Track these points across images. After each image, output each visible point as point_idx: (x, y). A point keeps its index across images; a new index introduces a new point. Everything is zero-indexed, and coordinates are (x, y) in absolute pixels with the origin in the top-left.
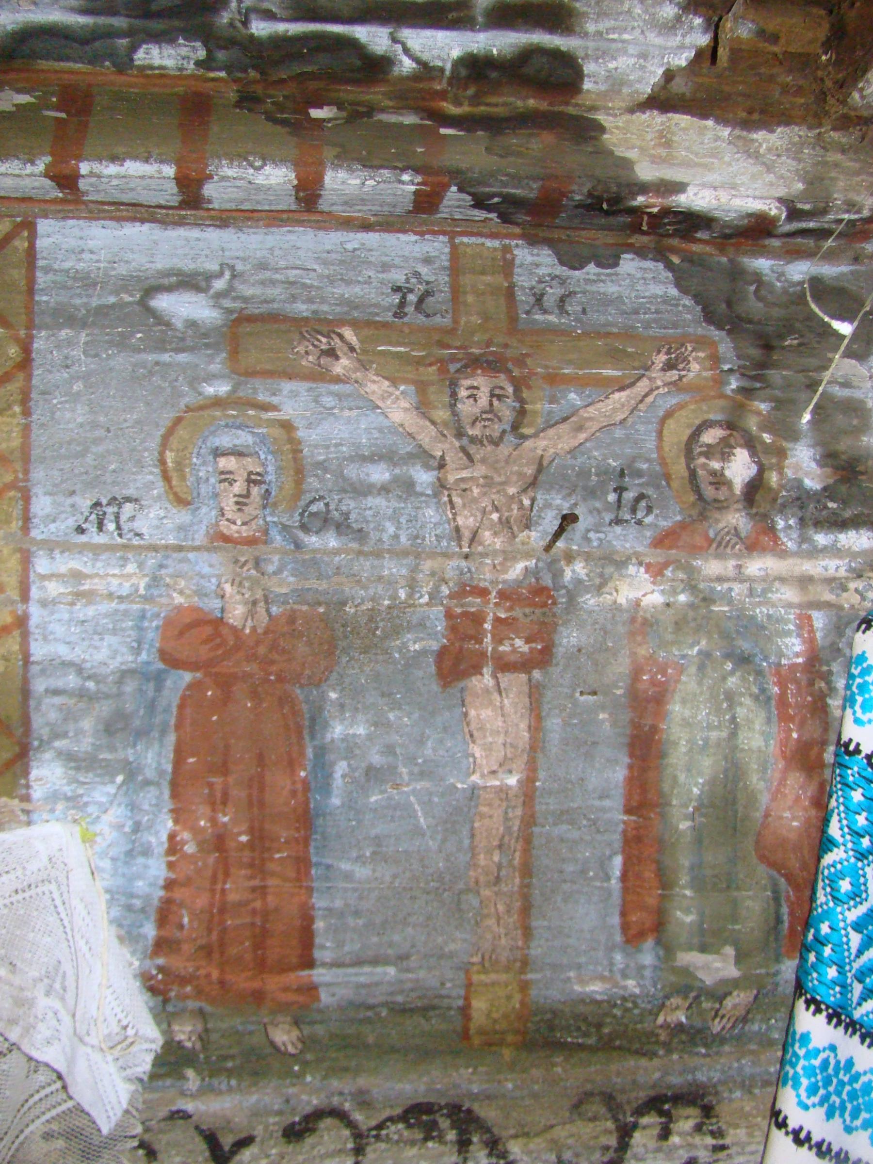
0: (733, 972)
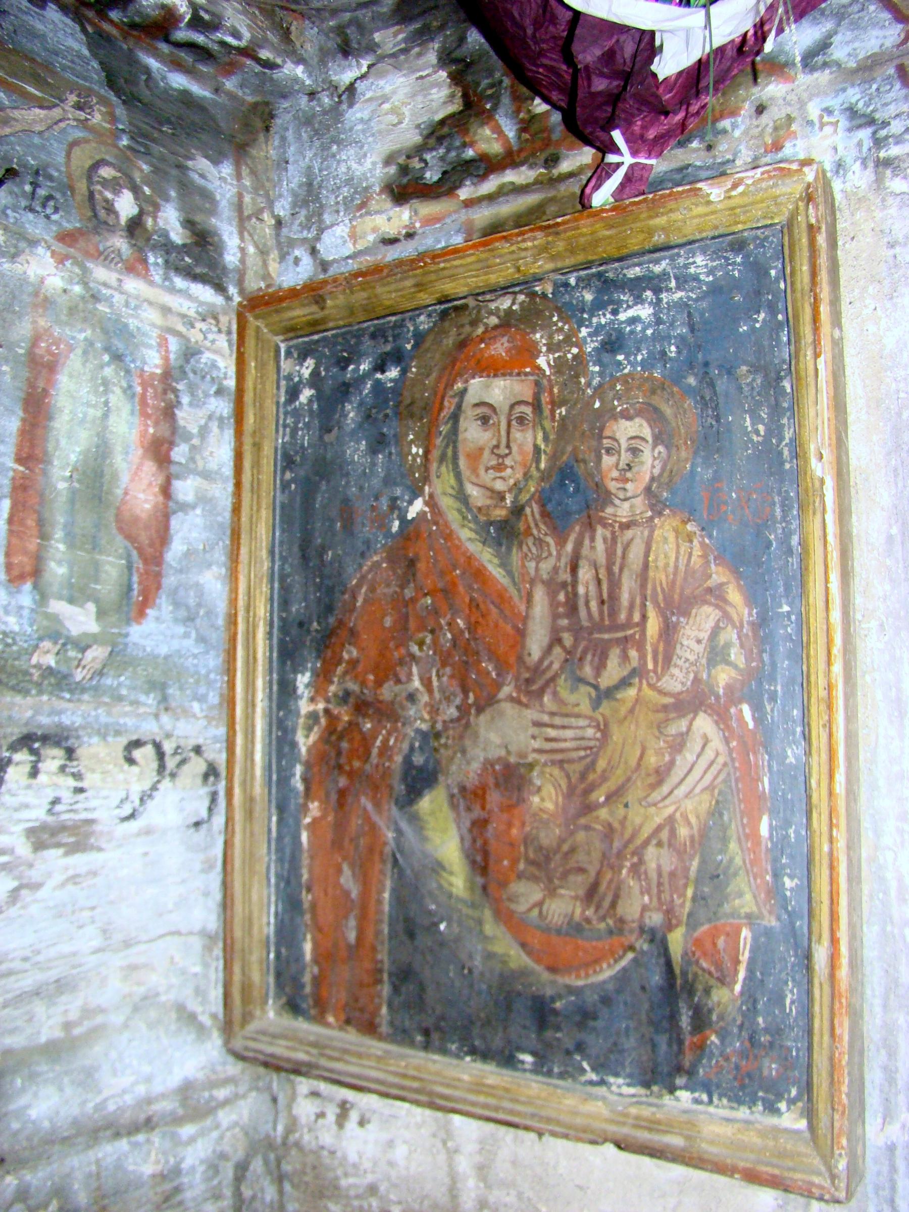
0: (93, 627)
